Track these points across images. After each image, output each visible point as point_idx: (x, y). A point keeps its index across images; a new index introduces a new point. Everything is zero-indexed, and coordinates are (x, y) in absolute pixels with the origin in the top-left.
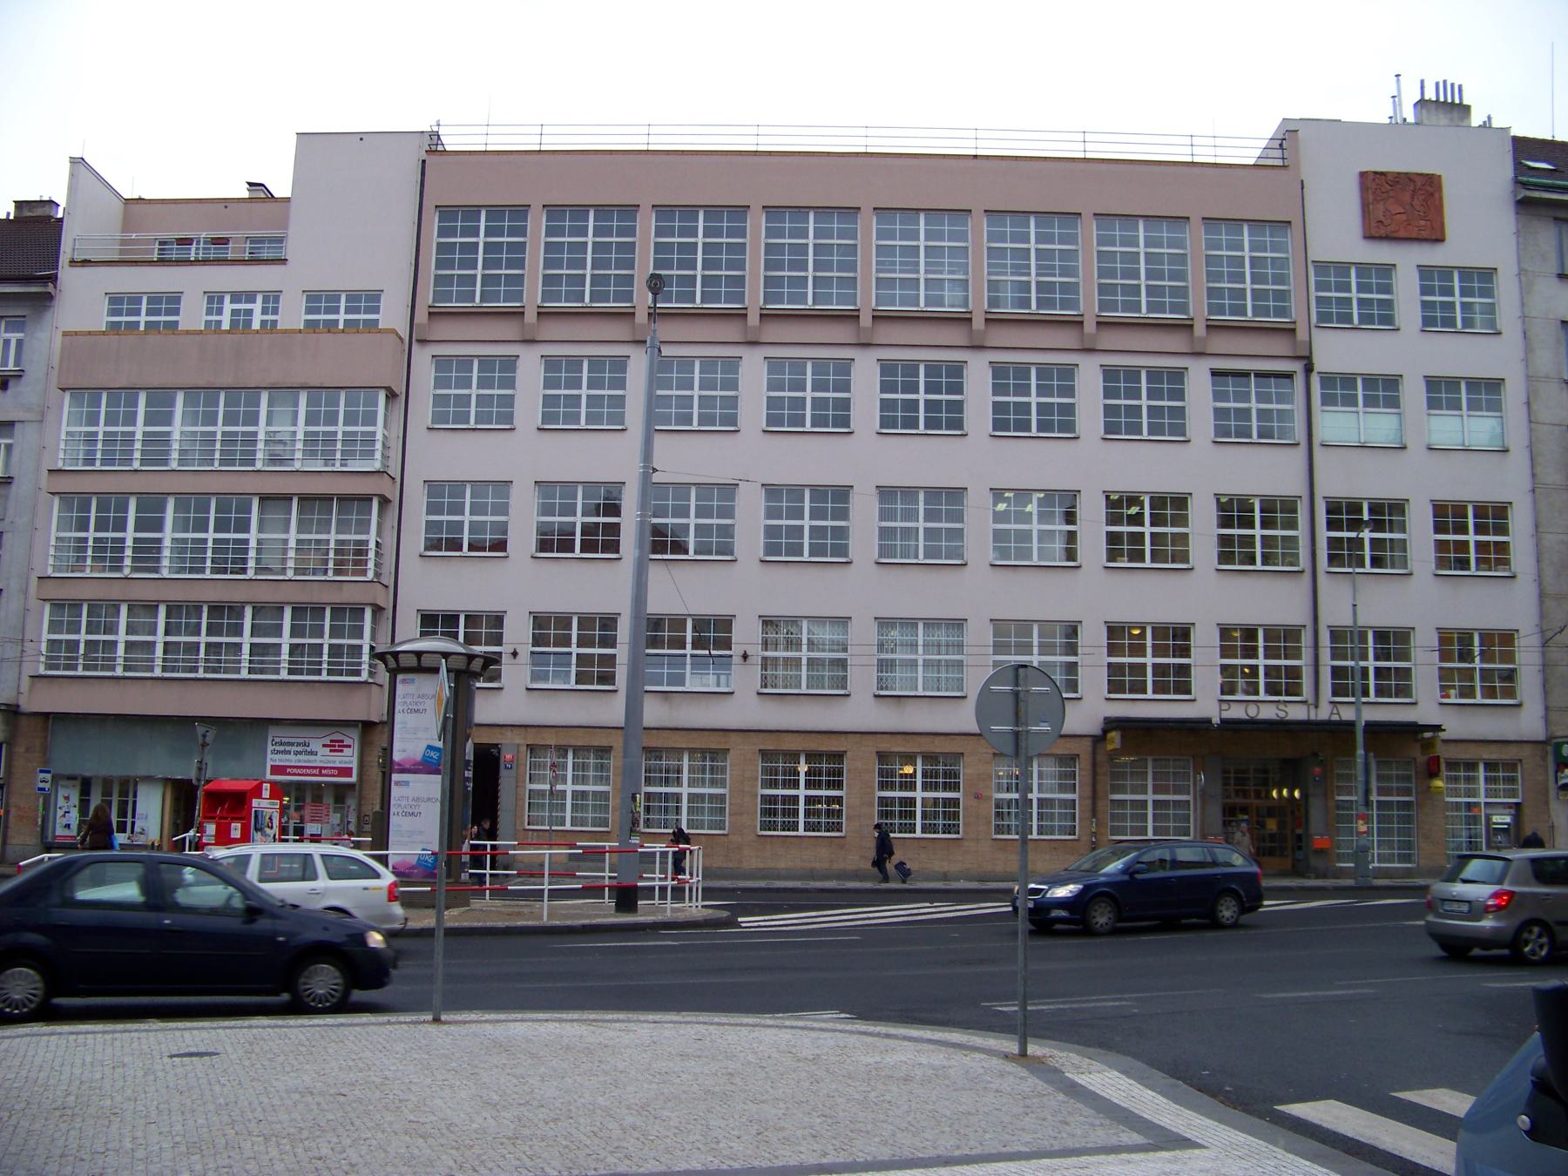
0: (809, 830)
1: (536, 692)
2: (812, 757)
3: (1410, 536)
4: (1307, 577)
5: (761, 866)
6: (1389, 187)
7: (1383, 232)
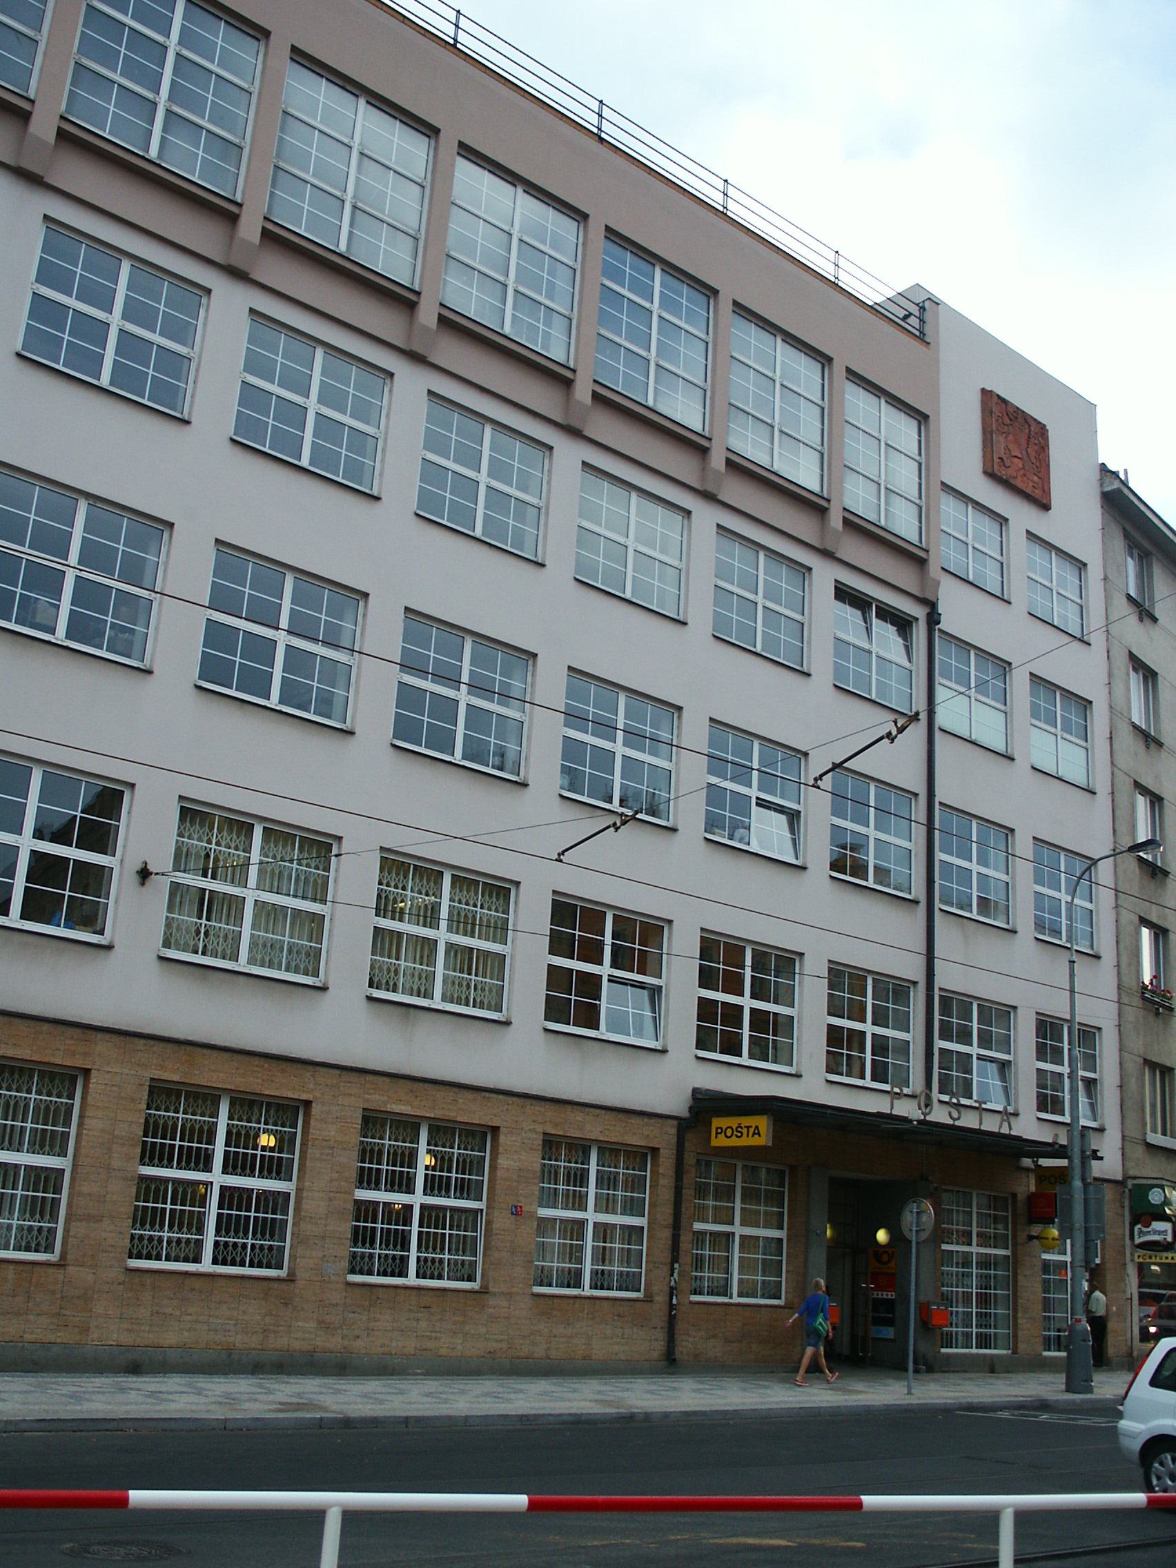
0: (224, 1263)
1: (561, 1036)
2: (441, 1131)
3: (806, 806)
4: (922, 907)
5: (126, 1339)
6: (1009, 422)
7: (1003, 473)
